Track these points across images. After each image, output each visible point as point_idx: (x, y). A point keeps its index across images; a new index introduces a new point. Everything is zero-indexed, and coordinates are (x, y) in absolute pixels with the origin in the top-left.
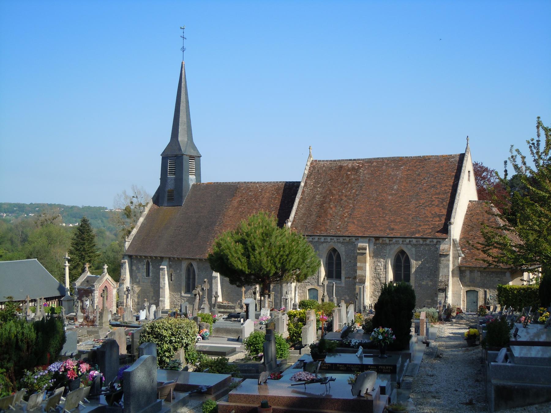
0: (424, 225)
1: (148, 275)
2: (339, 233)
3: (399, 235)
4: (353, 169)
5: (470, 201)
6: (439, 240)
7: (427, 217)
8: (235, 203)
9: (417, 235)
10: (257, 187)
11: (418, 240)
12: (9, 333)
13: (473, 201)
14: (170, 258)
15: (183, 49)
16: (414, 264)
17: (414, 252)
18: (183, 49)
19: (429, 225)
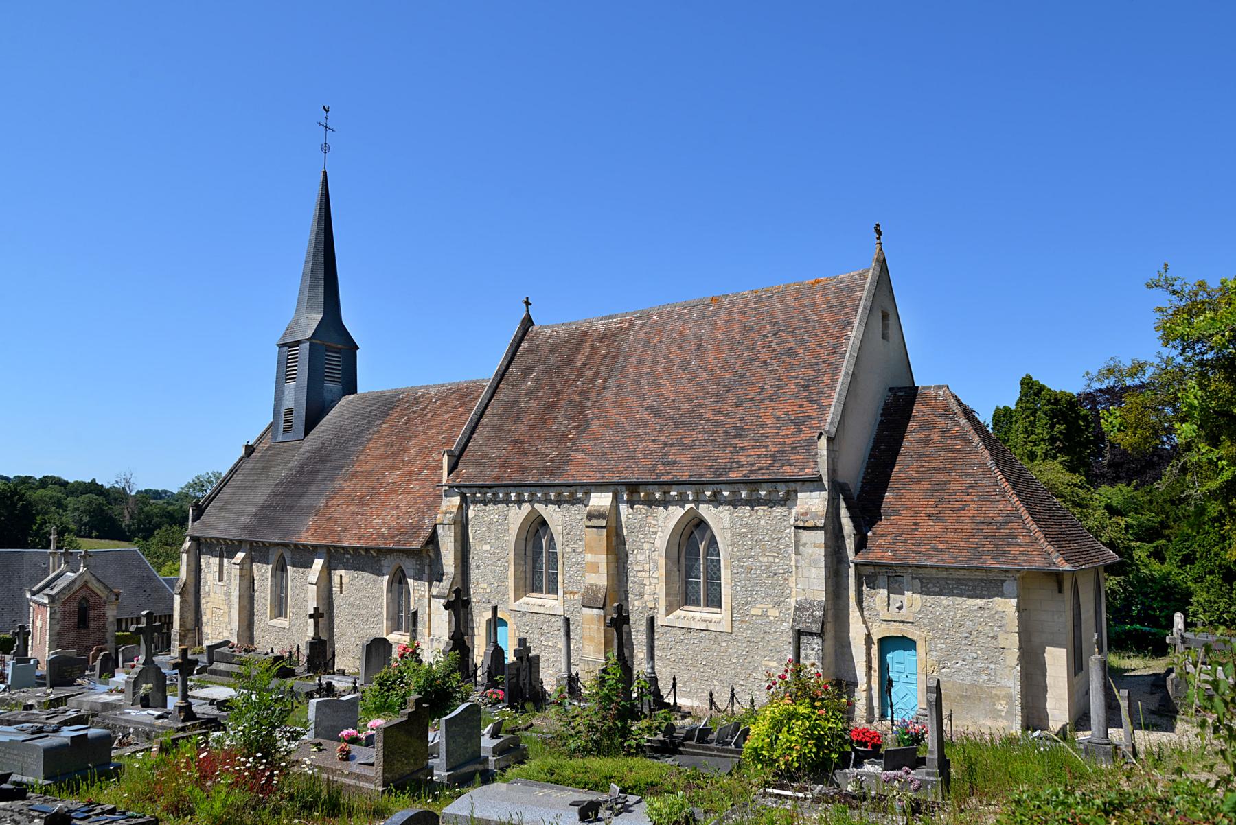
0: (753, 447)
1: (221, 580)
2: (546, 479)
3: (685, 477)
4: (608, 336)
5: (891, 389)
6: (793, 486)
7: (763, 426)
8: (385, 428)
9: (733, 476)
10: (988, 589)
11: (736, 487)
12: (992, 741)
13: (900, 389)
14: (251, 543)
15: (325, 148)
16: (1173, 675)
17: (727, 524)
18: (325, 148)
19: (766, 447)
